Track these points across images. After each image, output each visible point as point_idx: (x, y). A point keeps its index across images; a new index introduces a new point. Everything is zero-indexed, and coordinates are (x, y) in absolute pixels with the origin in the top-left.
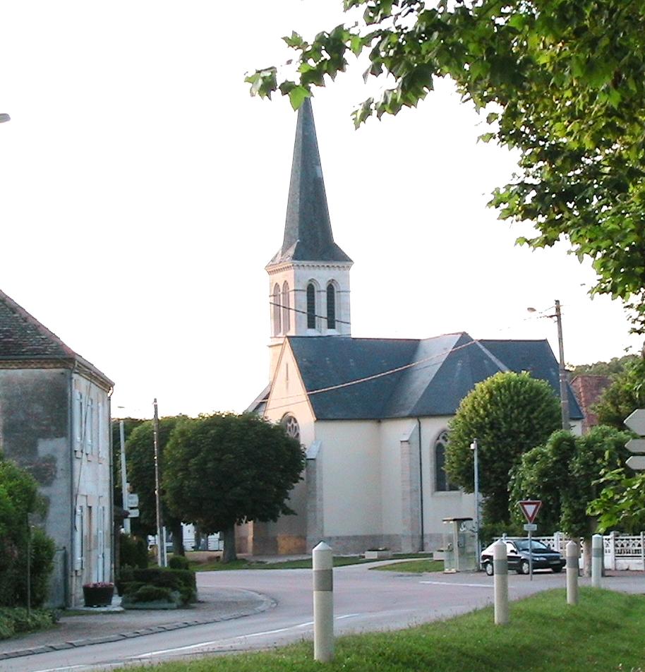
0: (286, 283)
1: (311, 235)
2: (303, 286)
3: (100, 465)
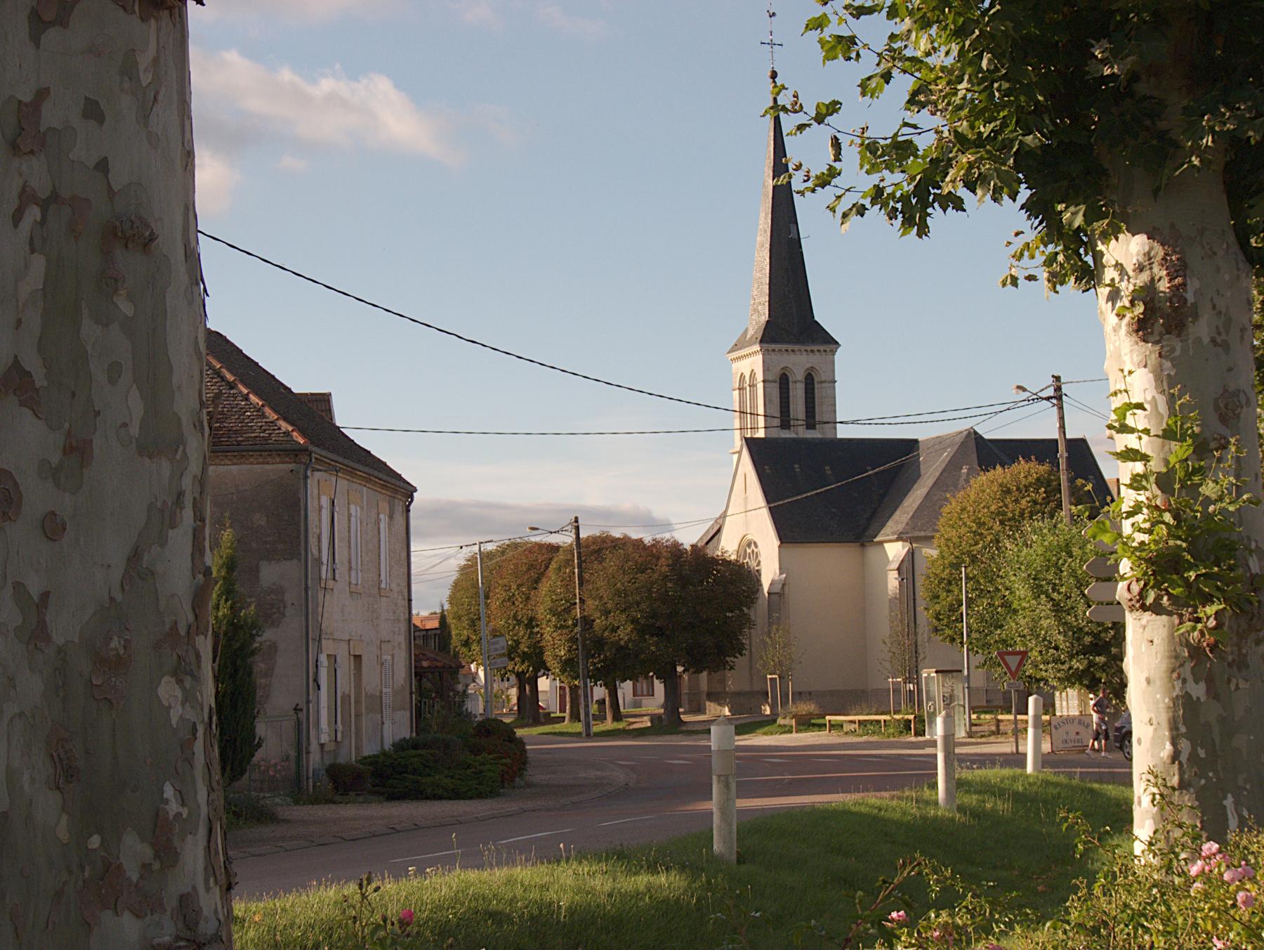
0: (752, 373)
1: (791, 320)
2: (777, 371)
3: (384, 599)
